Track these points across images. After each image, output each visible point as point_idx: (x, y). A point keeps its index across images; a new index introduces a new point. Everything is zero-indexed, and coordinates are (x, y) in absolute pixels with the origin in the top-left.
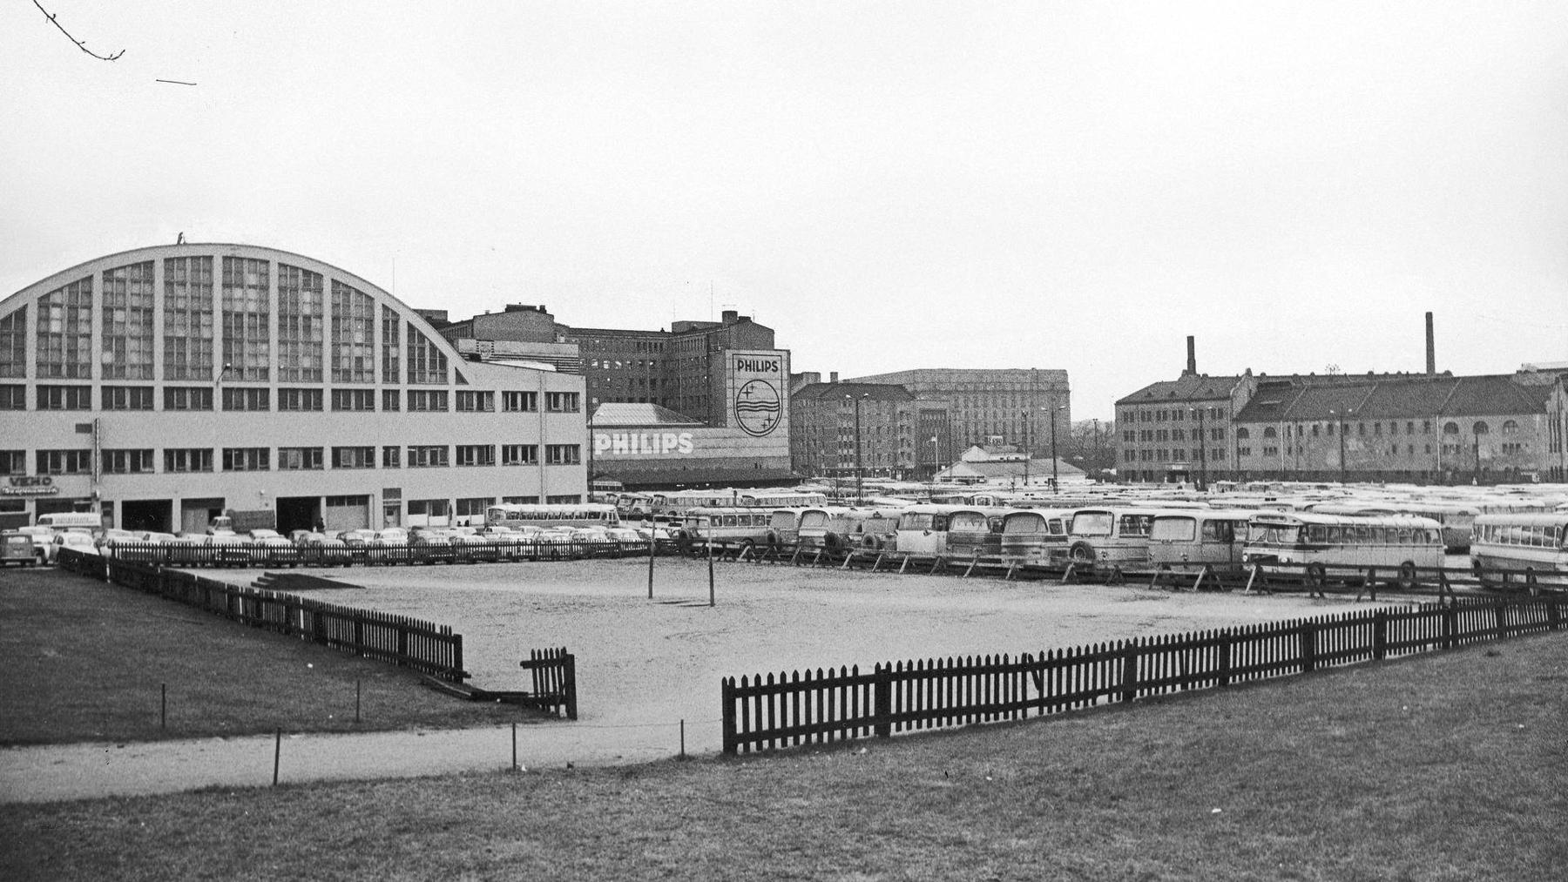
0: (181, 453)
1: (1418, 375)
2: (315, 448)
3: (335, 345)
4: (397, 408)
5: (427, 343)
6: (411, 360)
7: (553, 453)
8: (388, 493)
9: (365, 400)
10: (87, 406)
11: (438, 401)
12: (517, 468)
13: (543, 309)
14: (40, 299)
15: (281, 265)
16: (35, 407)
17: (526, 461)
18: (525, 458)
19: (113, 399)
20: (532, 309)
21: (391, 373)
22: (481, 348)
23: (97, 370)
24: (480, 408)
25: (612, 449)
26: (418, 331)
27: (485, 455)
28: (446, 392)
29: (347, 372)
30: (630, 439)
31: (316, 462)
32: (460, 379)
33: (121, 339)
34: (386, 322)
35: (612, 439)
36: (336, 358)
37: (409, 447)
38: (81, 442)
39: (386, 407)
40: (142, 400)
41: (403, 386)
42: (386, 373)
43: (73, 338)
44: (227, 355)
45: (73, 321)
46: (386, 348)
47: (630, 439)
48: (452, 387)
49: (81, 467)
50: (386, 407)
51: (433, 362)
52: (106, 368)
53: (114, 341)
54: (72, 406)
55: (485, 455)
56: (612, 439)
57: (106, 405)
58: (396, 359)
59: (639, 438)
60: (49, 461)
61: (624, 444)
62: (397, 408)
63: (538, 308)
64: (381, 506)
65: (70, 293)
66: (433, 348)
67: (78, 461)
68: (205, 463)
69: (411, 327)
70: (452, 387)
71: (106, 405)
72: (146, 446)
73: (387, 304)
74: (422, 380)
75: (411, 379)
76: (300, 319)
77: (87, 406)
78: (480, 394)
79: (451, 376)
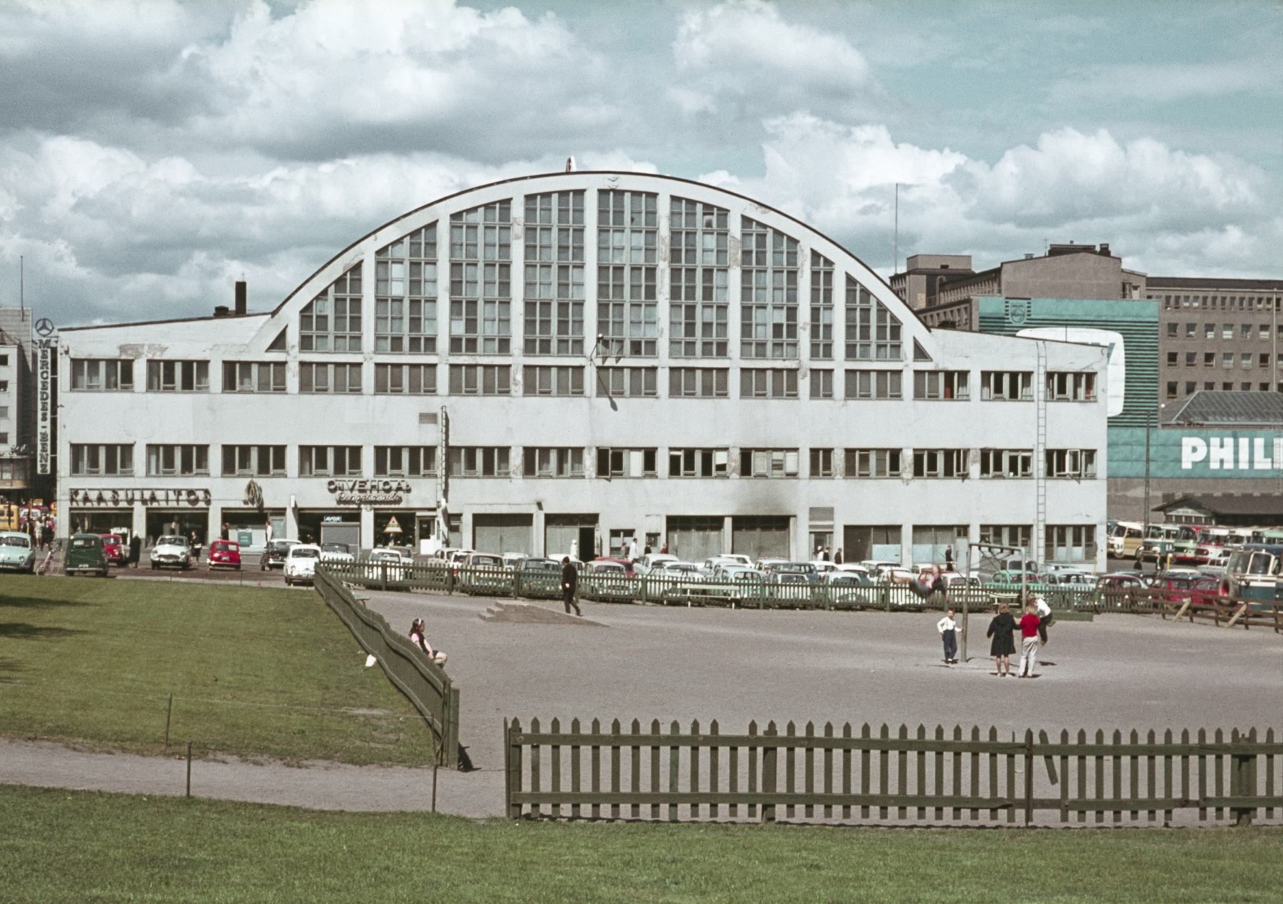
0: (865, 454)
1: (1007, 744)
2: (861, 450)
3: (746, 310)
4: (829, 395)
5: (873, 302)
6: (850, 329)
7: (1056, 461)
8: (815, 512)
9: (785, 384)
10: (432, 391)
11: (888, 385)
12: (1002, 482)
13: (1105, 251)
14: (378, 253)
15: (675, 199)
16: (372, 390)
17: (1016, 474)
18: (1013, 468)
19: (463, 381)
20: (1089, 249)
21: (822, 348)
22: (1011, 310)
23: (443, 344)
24: (950, 395)
25: (1207, 460)
26: (861, 285)
27: (925, 463)
28: (831, 371)
29: (761, 345)
30: (1236, 446)
31: (199, 466)
32: (920, 353)
33: (472, 304)
34: (815, 274)
35: (1208, 446)
36: (746, 329)
37: (671, 449)
38: (430, 436)
39: (814, 393)
40: (497, 381)
41: (839, 363)
42: (814, 347)
43: (415, 303)
44: (602, 325)
45: (415, 284)
46: (815, 312)
47: (1236, 446)
48: (908, 365)
49: (275, 467)
50: (814, 393)
51: (881, 329)
52: (455, 344)
53: (464, 308)
54: (415, 390)
55: (925, 463)
56: (1208, 446)
57: (454, 389)
58: (828, 327)
59: (1251, 446)
60: (387, 457)
61: (1227, 453)
62: (829, 395)
63: (1098, 249)
64: (807, 530)
65: (411, 244)
66: (882, 310)
67: (420, 458)
68: (123, 466)
69: (851, 281)
70: (908, 365)
71: (454, 389)
72: (201, 441)
73: (815, 249)
74: (864, 356)
75: (850, 352)
76: (699, 273)
77: (432, 391)
78: (949, 375)
79: (908, 349)
